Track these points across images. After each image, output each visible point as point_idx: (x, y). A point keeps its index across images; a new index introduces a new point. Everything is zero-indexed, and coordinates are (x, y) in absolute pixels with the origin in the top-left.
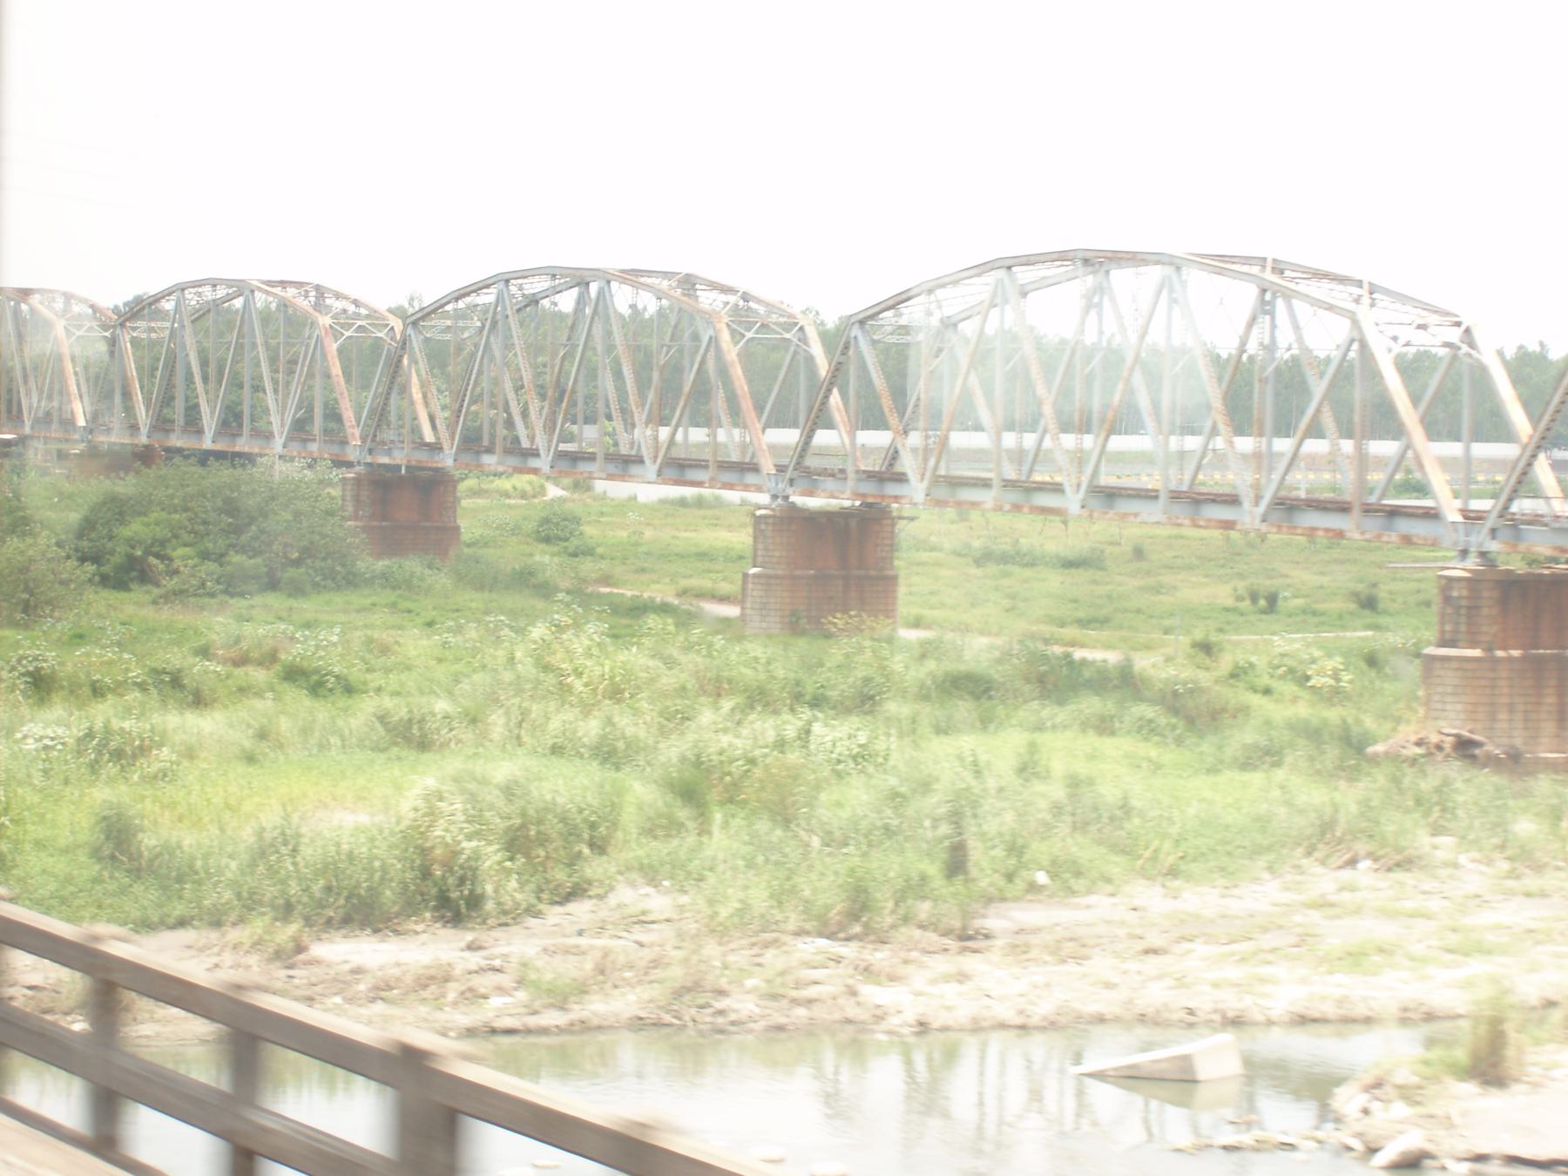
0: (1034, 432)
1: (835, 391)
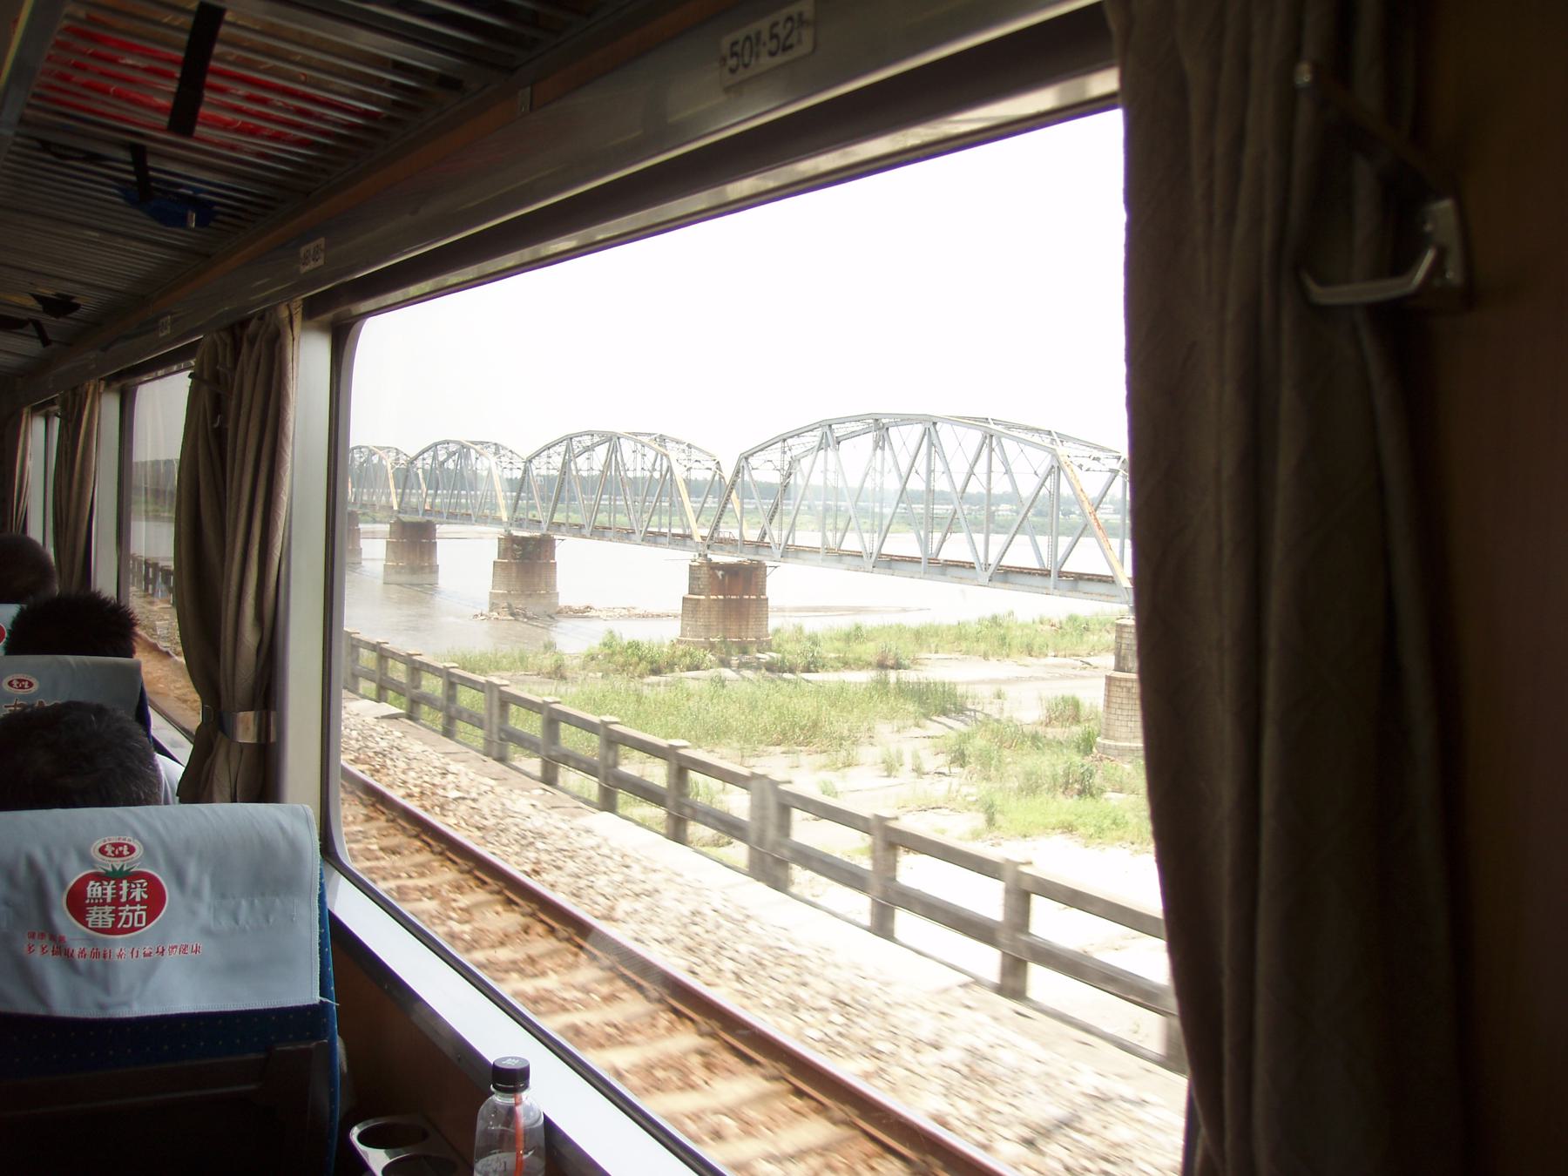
0: (1006, 533)
1: (734, 491)
